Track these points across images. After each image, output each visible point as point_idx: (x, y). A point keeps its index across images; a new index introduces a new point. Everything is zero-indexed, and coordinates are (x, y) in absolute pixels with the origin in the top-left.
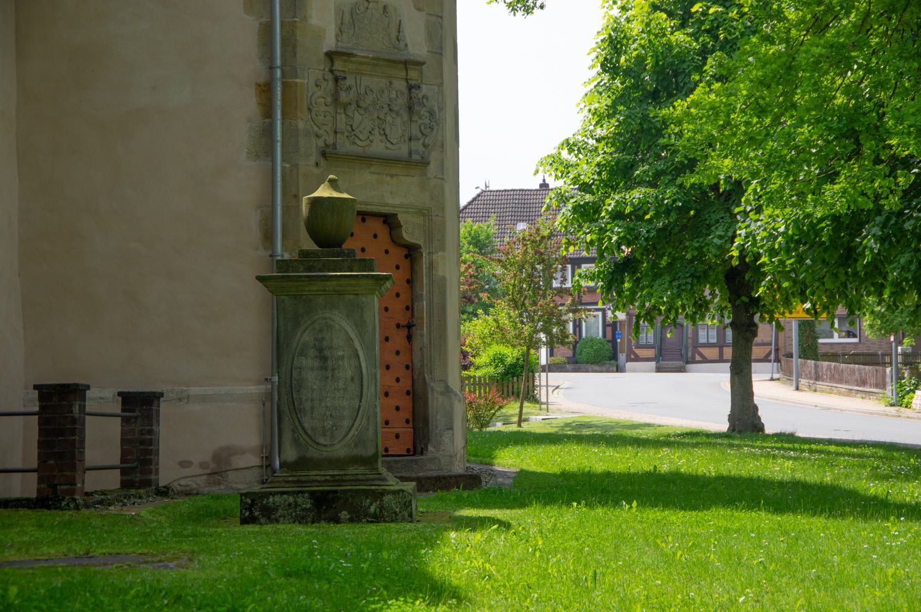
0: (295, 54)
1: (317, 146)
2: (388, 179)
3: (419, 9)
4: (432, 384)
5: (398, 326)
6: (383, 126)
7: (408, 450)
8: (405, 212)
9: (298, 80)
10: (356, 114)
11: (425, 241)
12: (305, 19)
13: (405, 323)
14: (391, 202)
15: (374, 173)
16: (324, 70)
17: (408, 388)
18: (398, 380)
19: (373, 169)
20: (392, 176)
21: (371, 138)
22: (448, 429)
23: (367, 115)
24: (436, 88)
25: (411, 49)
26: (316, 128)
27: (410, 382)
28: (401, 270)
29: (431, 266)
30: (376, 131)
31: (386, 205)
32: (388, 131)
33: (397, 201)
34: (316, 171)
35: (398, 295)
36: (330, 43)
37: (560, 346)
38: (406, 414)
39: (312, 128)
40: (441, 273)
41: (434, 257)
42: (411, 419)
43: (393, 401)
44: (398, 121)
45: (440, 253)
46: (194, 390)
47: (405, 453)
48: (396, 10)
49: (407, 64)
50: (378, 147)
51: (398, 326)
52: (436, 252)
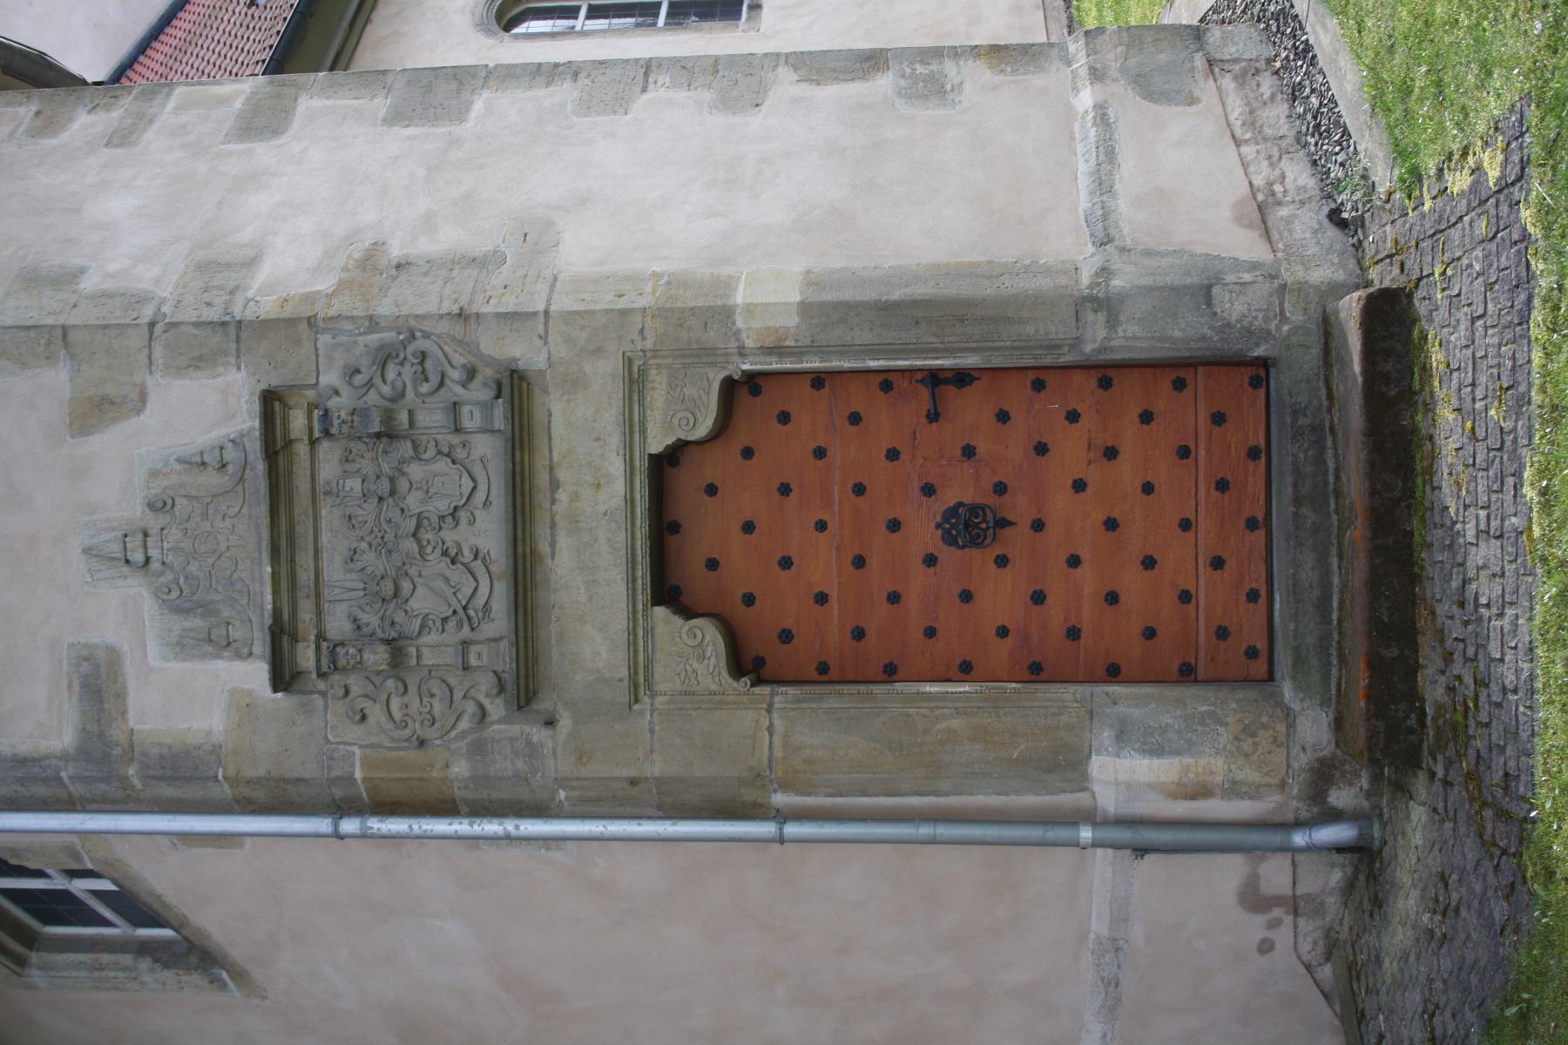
0: (299, 780)
1: (505, 720)
2: (562, 495)
3: (143, 398)
4: (1088, 348)
5: (934, 416)
6: (435, 519)
7: (1256, 383)
8: (643, 432)
9: (358, 775)
10: (414, 604)
11: (713, 365)
12: (216, 750)
13: (924, 393)
14: (619, 487)
15: (553, 544)
16: (323, 694)
17: (1094, 383)
18: (1073, 417)
19: (544, 547)
20: (555, 485)
21: (467, 555)
22: (1209, 303)
23: (413, 571)
24: (324, 339)
25: (246, 426)
26: (464, 724)
27: (1078, 378)
28: (793, 410)
29: (777, 350)
30: (449, 536)
31: (630, 501)
32: (443, 506)
33: (616, 466)
34: (565, 723)
35: (855, 419)
36: (254, 674)
37: (979, 500)
38: (1163, 399)
39: (463, 734)
40: (792, 321)
41: (750, 343)
42: (1174, 374)
43: (1129, 434)
44: (415, 471)
45: (740, 323)
46: (1099, 926)
47: (1262, 392)
48: (154, 474)
49: (275, 445)
50: (487, 533)
51: (934, 416)
52: (738, 333)
